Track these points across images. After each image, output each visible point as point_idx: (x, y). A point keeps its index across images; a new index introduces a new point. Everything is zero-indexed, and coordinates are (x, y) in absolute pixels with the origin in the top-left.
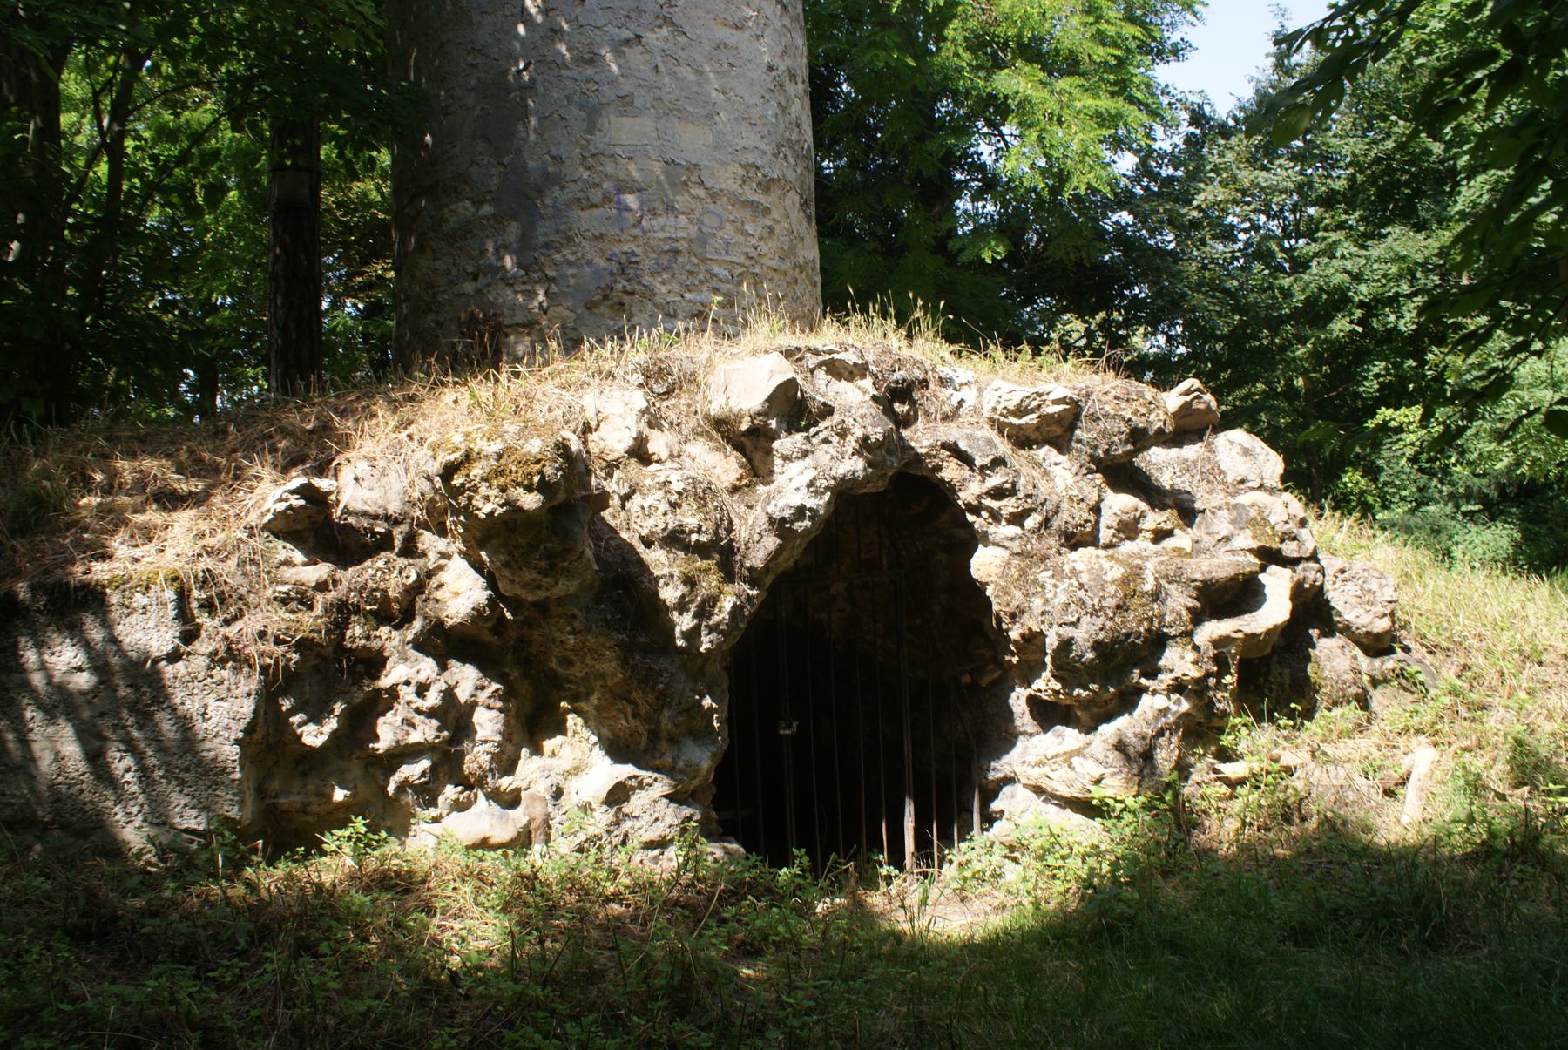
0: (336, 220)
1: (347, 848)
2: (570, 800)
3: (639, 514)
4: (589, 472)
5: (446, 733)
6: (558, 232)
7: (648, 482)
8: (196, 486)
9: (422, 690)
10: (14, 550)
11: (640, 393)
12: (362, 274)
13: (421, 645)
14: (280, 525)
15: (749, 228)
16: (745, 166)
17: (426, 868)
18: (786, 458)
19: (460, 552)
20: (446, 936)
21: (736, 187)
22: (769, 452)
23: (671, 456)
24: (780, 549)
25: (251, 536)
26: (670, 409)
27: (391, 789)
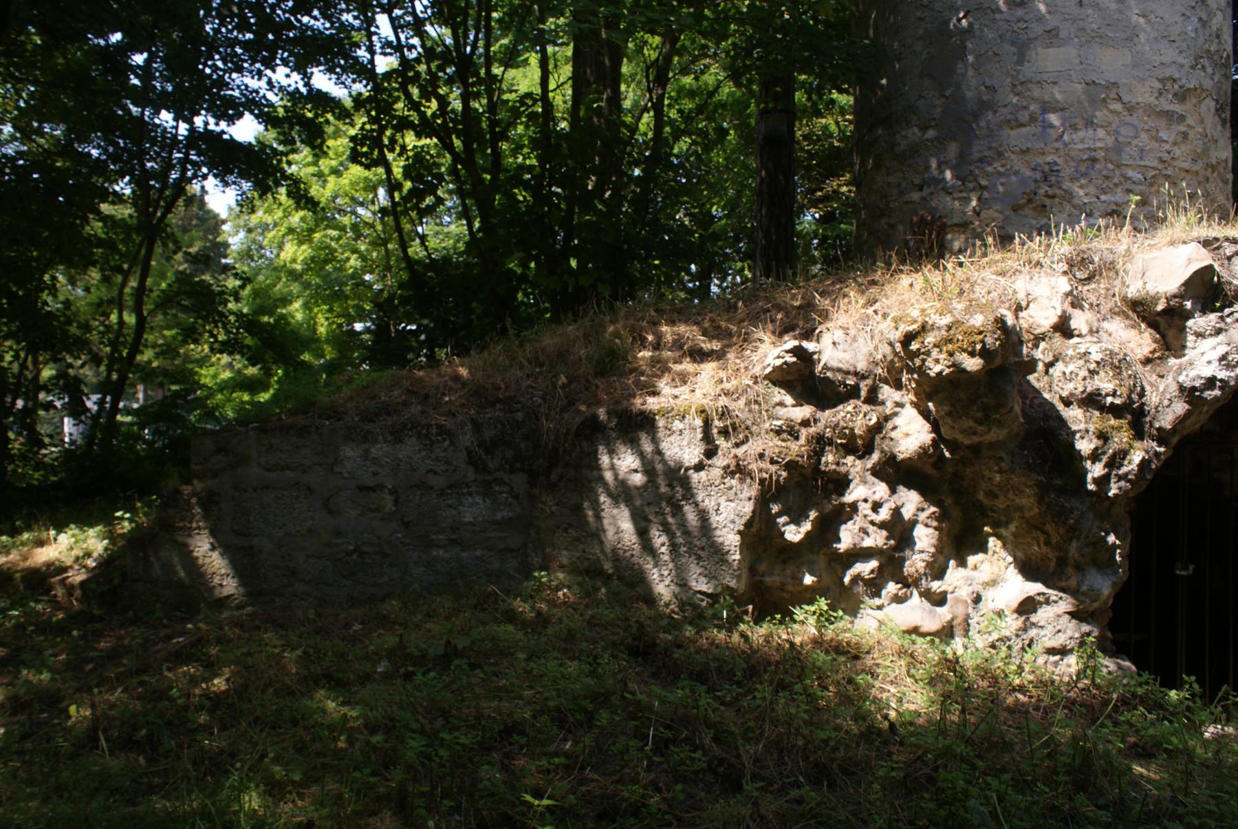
0: (802, 149)
1: (812, 620)
2: (988, 605)
3: (1060, 379)
4: (1021, 343)
5: (892, 542)
6: (990, 148)
7: (1070, 352)
8: (716, 345)
9: (876, 507)
10: (597, 386)
11: (1065, 279)
12: (821, 190)
13: (877, 472)
14: (777, 376)
15: (1163, 135)
16: (1162, 81)
17: (871, 643)
18: (1199, 335)
19: (912, 403)
20: (884, 696)
21: (1152, 99)
22: (1182, 330)
23: (1091, 332)
24: (1188, 415)
25: (756, 383)
26: (1089, 292)
27: (847, 580)
